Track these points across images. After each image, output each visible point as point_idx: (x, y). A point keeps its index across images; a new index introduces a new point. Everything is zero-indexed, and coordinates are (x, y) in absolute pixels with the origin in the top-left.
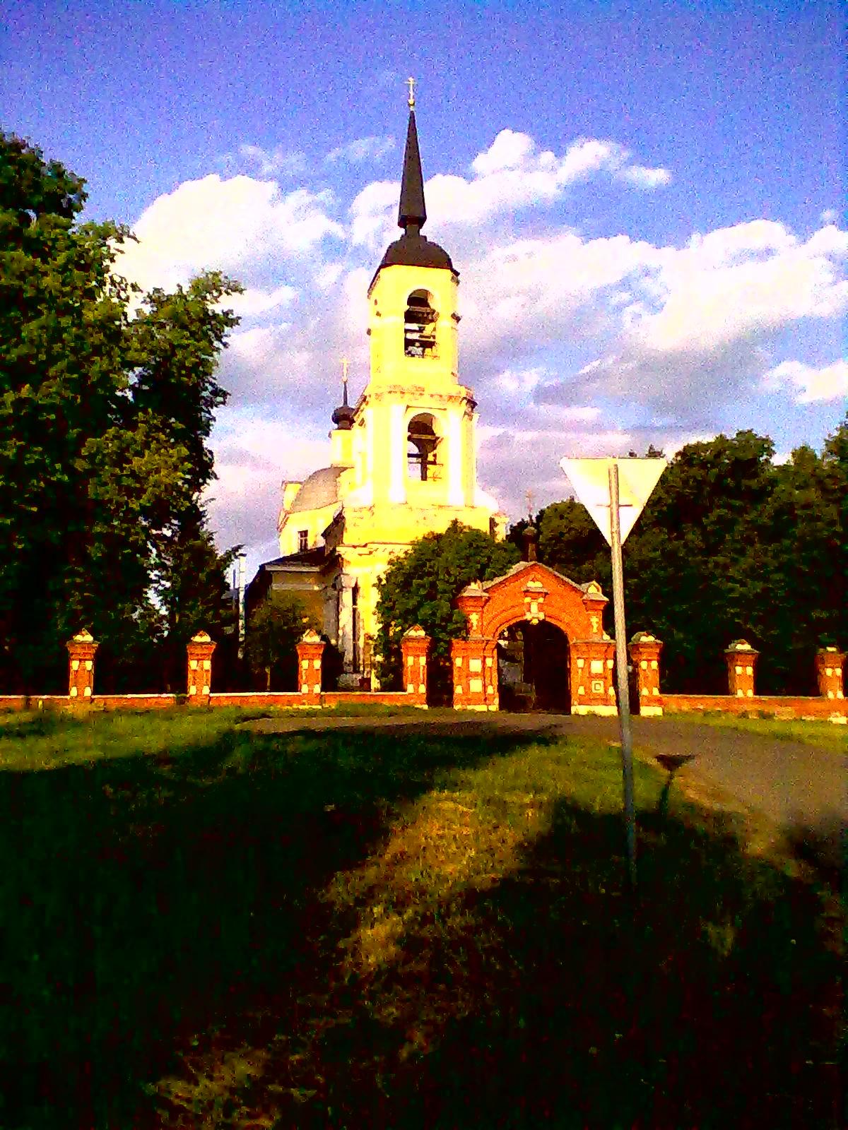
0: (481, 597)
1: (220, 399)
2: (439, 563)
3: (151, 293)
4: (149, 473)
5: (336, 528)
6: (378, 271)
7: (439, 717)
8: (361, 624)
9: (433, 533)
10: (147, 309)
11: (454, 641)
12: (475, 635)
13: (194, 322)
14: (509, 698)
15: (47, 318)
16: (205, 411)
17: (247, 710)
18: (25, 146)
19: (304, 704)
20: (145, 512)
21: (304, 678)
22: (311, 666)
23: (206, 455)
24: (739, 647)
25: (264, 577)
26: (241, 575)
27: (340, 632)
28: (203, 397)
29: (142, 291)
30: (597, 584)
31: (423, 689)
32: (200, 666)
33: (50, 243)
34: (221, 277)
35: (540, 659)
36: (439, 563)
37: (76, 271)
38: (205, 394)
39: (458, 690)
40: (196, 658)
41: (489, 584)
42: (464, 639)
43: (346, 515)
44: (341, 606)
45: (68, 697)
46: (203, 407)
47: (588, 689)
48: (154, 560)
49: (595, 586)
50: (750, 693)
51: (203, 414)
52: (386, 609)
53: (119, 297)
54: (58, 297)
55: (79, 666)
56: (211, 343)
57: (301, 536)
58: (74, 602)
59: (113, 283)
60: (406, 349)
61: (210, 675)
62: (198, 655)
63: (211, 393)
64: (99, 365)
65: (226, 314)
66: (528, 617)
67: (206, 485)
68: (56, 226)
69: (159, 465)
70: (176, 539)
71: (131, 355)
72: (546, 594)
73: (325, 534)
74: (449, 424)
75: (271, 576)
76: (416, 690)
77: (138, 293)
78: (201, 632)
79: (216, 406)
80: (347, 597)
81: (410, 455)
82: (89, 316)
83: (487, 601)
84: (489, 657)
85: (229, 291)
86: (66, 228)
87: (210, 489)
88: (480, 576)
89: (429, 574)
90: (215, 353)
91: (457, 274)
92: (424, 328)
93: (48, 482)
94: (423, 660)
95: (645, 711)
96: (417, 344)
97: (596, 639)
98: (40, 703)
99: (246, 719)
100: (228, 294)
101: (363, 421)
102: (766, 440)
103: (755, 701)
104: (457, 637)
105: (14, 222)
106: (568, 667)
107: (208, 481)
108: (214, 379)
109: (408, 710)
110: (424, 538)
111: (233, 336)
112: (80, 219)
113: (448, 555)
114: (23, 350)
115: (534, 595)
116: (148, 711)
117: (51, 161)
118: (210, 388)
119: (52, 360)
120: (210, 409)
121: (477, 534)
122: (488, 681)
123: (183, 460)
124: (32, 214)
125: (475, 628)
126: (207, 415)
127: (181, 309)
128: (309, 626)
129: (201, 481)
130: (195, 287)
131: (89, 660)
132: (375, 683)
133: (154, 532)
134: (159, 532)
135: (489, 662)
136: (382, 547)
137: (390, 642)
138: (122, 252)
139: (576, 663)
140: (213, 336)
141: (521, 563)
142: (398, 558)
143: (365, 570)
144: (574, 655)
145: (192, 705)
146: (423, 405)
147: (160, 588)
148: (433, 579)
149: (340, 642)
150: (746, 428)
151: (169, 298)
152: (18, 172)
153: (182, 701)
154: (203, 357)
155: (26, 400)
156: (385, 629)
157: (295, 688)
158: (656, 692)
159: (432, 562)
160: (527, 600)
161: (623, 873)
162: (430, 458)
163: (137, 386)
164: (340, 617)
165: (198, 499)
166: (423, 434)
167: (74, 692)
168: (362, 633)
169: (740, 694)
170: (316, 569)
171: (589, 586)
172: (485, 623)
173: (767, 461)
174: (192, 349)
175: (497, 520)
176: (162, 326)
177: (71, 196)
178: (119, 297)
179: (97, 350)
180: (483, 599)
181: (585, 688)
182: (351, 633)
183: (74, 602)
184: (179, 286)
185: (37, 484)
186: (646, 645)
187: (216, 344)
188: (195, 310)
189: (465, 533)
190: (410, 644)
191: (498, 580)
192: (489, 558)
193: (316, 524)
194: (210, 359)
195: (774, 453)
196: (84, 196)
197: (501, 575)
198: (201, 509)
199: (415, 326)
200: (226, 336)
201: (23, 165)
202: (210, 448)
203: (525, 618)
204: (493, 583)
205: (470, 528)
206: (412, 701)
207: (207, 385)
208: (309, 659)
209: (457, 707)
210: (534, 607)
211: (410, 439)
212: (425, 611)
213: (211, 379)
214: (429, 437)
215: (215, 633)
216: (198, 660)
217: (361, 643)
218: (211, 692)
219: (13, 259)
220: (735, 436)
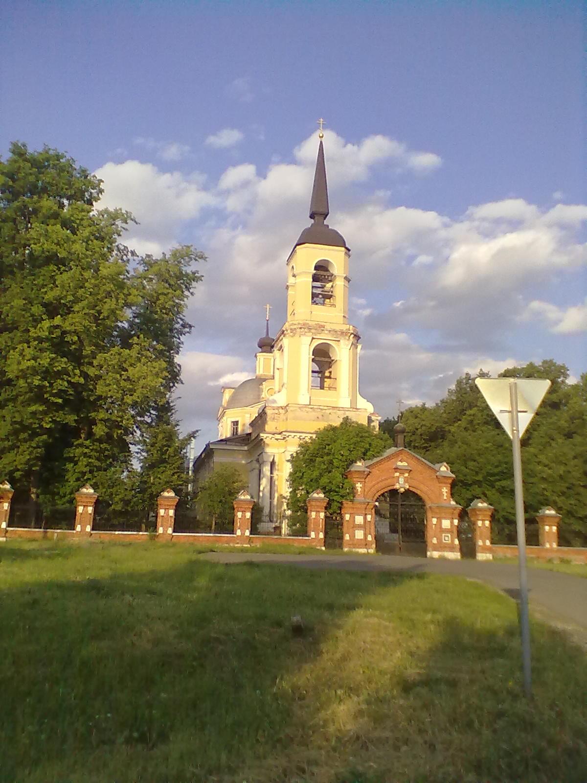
0: (364, 471)
1: (187, 330)
2: (334, 447)
3: (144, 257)
4: (139, 379)
5: (260, 420)
6: (295, 247)
7: (333, 557)
8: (276, 488)
9: (331, 426)
10: (141, 268)
11: (344, 502)
12: (359, 498)
13: (175, 277)
14: (382, 545)
15: (75, 271)
16: (176, 338)
17: (199, 546)
18: (63, 156)
19: (238, 543)
20: (134, 405)
21: (239, 524)
22: (244, 516)
23: (176, 367)
24: (547, 512)
25: (208, 452)
26: (194, 451)
27: (261, 494)
28: (176, 329)
29: (138, 256)
30: (446, 465)
31: (321, 535)
32: (166, 513)
33: (78, 222)
34: (192, 249)
35: (404, 518)
36: (334, 447)
37: (95, 241)
38: (177, 326)
39: (347, 537)
40: (164, 507)
41: (369, 463)
42: (352, 501)
43: (269, 412)
44: (262, 476)
45: (74, 532)
46: (176, 335)
47: (439, 540)
48: (138, 438)
49: (445, 466)
50: (555, 545)
51: (175, 339)
52: (295, 479)
53: (122, 259)
54: (83, 258)
55: (83, 510)
56: (183, 292)
57: (234, 425)
58: (82, 466)
59: (119, 250)
60: (313, 298)
61: (173, 520)
62: (165, 505)
63: (182, 325)
64: (110, 304)
65: (194, 273)
66: (397, 486)
67: (174, 387)
68: (83, 210)
69: (145, 373)
70: (154, 424)
71: (130, 299)
72: (411, 471)
73: (252, 424)
74: (343, 354)
75: (213, 452)
76: (316, 535)
77: (135, 258)
78: (168, 490)
79: (184, 334)
80: (266, 469)
81: (313, 372)
82: (104, 272)
83: (368, 474)
84: (369, 514)
85: (197, 258)
86: (89, 212)
87: (178, 390)
88: (364, 456)
89: (328, 454)
90: (185, 299)
91: (349, 250)
92: (325, 286)
93: (69, 382)
94: (322, 515)
95: (481, 556)
96: (320, 296)
97: (445, 504)
98: (56, 535)
99: (200, 552)
100: (196, 260)
101: (281, 347)
102: (563, 367)
103: (558, 551)
104: (347, 499)
105: (56, 208)
106: (425, 523)
107: (176, 384)
108: (184, 316)
109: (312, 550)
110: (325, 429)
111: (199, 288)
112: (98, 206)
113: (342, 441)
114: (57, 292)
115: (402, 471)
116: (130, 544)
117: (80, 167)
118: (181, 322)
119: (77, 300)
120: (180, 337)
121: (361, 426)
122: (368, 532)
123: (162, 370)
124: (66, 202)
125: (359, 493)
126: (178, 340)
127: (163, 269)
128: (243, 488)
129: (171, 385)
130: (174, 255)
131: (90, 506)
132: (285, 529)
133: (139, 419)
134: (142, 419)
135: (369, 518)
136: (293, 434)
137: (298, 501)
138: (126, 230)
139: (431, 521)
140: (184, 287)
141: (393, 448)
142: (306, 442)
143: (281, 452)
144: (429, 514)
145: (161, 541)
146: (324, 338)
147: (142, 458)
148: (329, 459)
149: (260, 500)
150: (548, 359)
151: (156, 262)
152: (59, 175)
153: (153, 538)
154: (177, 301)
155: (57, 327)
156: (294, 492)
157: (232, 532)
158: (488, 543)
159: (330, 447)
160: (397, 474)
161: (487, 678)
162: (327, 374)
163: (131, 320)
164: (261, 482)
165: (170, 397)
166: (322, 358)
167: (78, 528)
168: (276, 495)
169: (548, 546)
170: (246, 448)
171: (441, 466)
172: (366, 490)
173: (563, 382)
174: (170, 296)
175: (373, 418)
176: (151, 280)
177: (92, 191)
178: (122, 259)
179: (109, 294)
180: (366, 473)
181: (437, 539)
182: (268, 495)
183: (82, 466)
184: (163, 253)
185: (61, 384)
186: (481, 510)
187: (186, 293)
188: (173, 270)
189: (353, 426)
190: (313, 503)
191: (375, 460)
192: (370, 445)
193: (245, 416)
194: (182, 302)
195: (568, 375)
196: (101, 191)
197: (378, 456)
198: (171, 404)
199: (318, 284)
200: (193, 288)
201: (62, 170)
202: (178, 363)
203: (395, 487)
204: (374, 462)
205: (357, 423)
206: (314, 544)
207: (179, 320)
208: (242, 512)
209: (346, 549)
210: (401, 480)
211: (313, 360)
212: (324, 481)
213: (181, 316)
214: (326, 360)
215: (177, 492)
216: (165, 509)
217: (275, 502)
218: (174, 532)
219: (53, 231)
220: (541, 364)
